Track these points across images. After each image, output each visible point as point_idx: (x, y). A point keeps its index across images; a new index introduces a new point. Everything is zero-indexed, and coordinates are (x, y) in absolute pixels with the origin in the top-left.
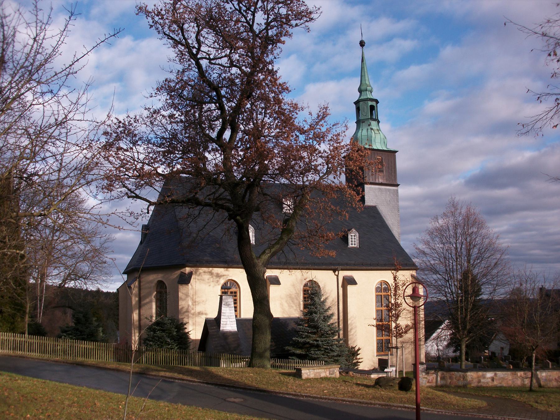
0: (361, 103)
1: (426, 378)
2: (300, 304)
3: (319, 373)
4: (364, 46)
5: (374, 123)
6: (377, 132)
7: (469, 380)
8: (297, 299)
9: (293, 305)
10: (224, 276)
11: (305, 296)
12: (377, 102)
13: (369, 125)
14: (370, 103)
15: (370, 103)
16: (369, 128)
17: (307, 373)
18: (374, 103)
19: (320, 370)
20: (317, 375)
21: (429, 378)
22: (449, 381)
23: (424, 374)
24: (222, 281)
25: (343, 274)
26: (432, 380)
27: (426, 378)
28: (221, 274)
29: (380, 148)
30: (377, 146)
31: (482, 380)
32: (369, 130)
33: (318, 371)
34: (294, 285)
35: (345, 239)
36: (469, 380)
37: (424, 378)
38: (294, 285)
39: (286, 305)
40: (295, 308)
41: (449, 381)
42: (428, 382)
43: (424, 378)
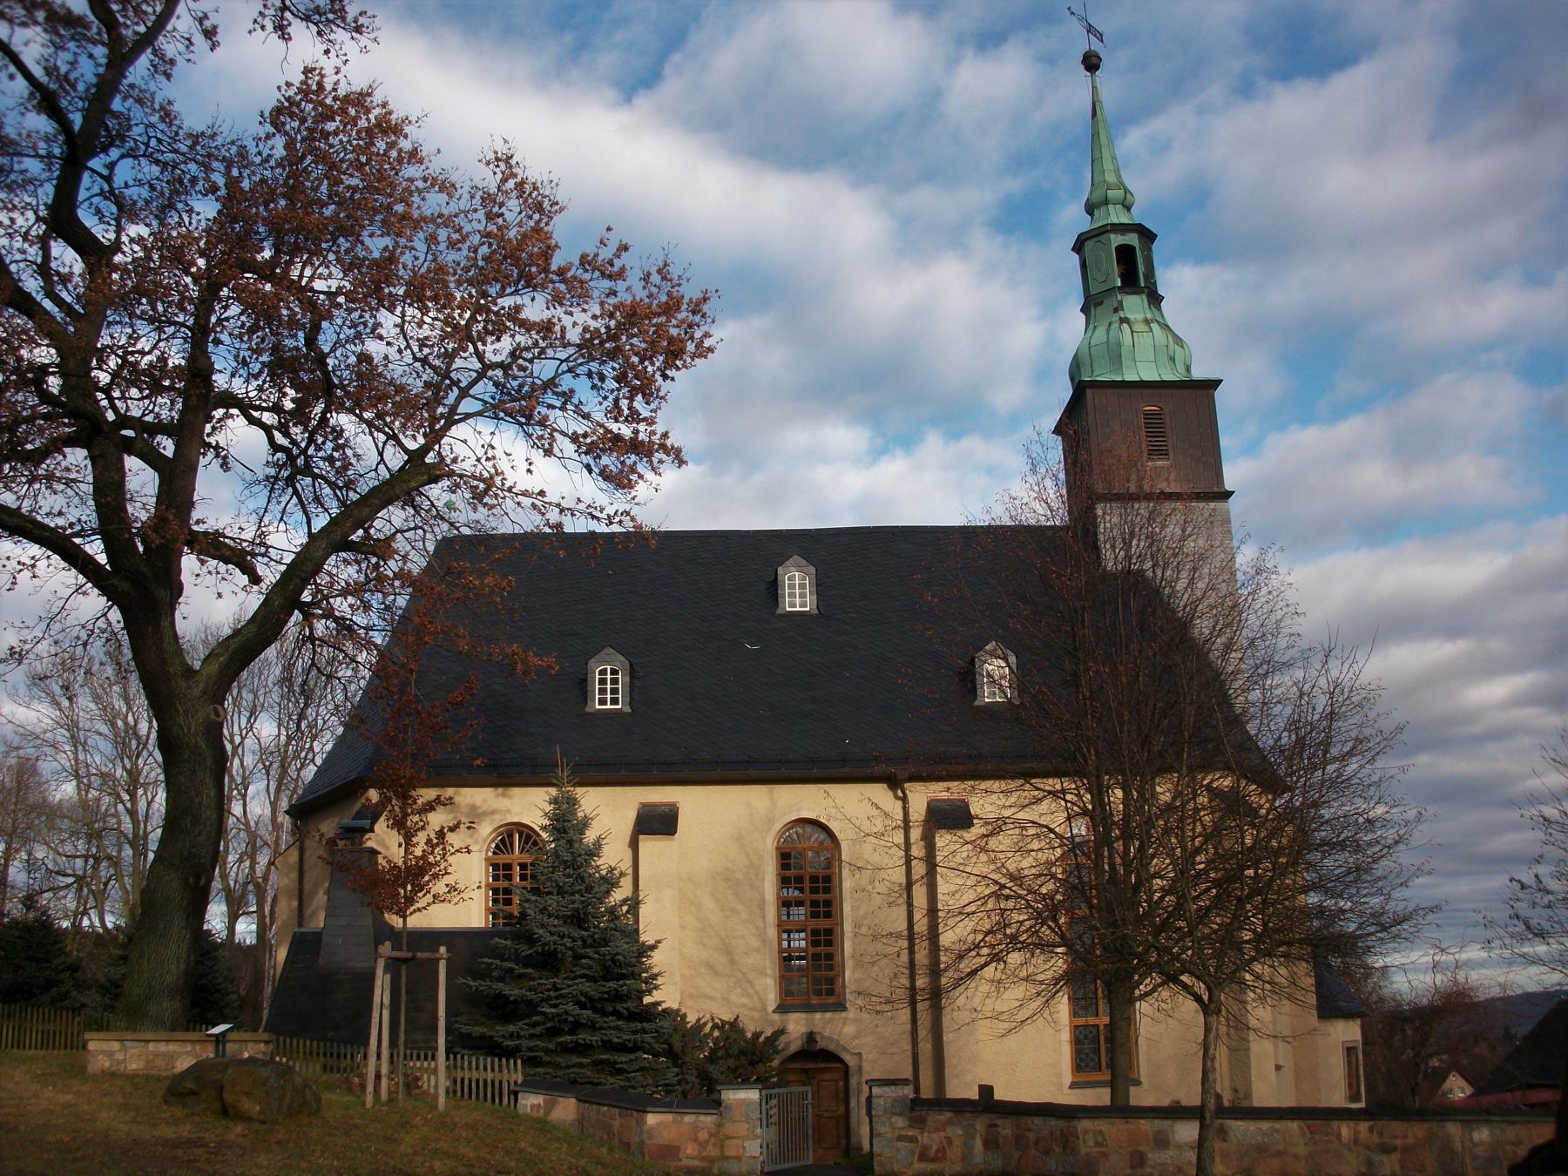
0: (1089, 245)
1: (912, 1140)
2: (762, 903)
3: (172, 1057)
4: (1097, 67)
5: (1134, 305)
6: (1143, 327)
7: (1083, 1151)
8: (752, 886)
9: (740, 907)
10: (493, 812)
11: (788, 873)
12: (1148, 236)
13: (1116, 310)
14: (1116, 240)
15: (1116, 240)
16: (1115, 318)
17: (110, 1054)
18: (1132, 239)
19: (172, 1047)
20: (160, 1062)
21: (925, 1139)
22: (1016, 1155)
23: (900, 1122)
24: (486, 829)
25: (921, 796)
26: (942, 1150)
27: (912, 1140)
28: (485, 807)
29: (1149, 374)
30: (1145, 370)
31: (1155, 1156)
32: (1115, 325)
33: (162, 1047)
34: (739, 839)
35: (969, 679)
36: (1083, 1151)
37: (900, 1138)
38: (739, 839)
39: (709, 903)
40: (744, 916)
41: (1016, 1155)
42: (923, 1157)
43: (900, 1138)
